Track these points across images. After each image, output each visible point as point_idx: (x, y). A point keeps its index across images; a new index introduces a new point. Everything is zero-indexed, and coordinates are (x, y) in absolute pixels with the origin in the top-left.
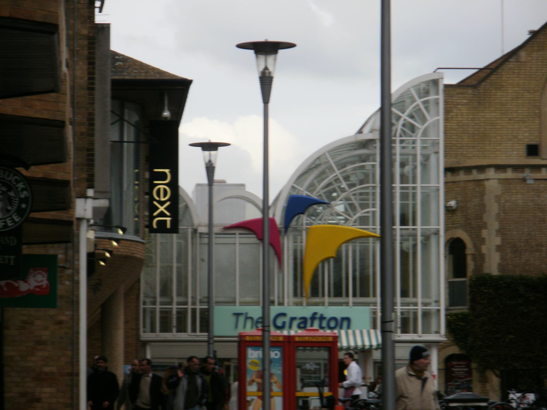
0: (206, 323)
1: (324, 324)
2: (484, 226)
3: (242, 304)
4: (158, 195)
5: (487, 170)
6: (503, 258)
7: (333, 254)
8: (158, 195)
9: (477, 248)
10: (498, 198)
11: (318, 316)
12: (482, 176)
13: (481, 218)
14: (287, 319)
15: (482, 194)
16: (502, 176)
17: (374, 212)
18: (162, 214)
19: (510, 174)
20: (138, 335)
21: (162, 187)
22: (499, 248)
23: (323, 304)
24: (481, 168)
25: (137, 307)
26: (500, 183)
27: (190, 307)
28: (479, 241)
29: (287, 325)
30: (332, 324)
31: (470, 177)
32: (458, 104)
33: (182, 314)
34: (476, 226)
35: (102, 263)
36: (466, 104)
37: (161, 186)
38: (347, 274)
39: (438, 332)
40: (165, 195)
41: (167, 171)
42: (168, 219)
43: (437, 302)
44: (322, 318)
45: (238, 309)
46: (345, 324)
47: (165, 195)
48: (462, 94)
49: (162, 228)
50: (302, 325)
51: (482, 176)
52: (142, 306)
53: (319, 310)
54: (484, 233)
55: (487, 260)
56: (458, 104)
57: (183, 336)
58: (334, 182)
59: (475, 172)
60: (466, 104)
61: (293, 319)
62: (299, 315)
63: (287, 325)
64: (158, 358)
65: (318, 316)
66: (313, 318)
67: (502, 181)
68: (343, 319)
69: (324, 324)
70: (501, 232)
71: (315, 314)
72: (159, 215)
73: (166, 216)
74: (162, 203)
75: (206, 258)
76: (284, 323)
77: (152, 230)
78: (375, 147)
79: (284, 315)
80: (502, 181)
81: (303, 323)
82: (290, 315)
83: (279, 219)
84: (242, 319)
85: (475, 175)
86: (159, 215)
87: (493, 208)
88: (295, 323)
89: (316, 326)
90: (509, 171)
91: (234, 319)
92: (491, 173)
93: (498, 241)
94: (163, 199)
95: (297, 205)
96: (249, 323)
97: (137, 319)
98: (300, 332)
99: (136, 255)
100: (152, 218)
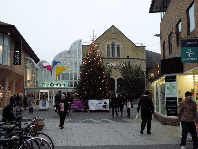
1: (60, 85)
7: (52, 70)
18: (17, 61)
35: (123, 103)
37: (17, 55)
38: (7, 57)
41: (19, 52)
44: (59, 84)
49: (17, 64)
66: (58, 84)
69: (60, 85)
72: (16, 61)
74: (17, 58)
77: (15, 64)
78: (179, 104)
82: (53, 83)
83: (51, 66)
84: (44, 84)
86: (16, 61)
88: (54, 85)
89: (58, 85)
95: (55, 63)
96: (45, 85)
97: (23, 85)
98: (55, 87)
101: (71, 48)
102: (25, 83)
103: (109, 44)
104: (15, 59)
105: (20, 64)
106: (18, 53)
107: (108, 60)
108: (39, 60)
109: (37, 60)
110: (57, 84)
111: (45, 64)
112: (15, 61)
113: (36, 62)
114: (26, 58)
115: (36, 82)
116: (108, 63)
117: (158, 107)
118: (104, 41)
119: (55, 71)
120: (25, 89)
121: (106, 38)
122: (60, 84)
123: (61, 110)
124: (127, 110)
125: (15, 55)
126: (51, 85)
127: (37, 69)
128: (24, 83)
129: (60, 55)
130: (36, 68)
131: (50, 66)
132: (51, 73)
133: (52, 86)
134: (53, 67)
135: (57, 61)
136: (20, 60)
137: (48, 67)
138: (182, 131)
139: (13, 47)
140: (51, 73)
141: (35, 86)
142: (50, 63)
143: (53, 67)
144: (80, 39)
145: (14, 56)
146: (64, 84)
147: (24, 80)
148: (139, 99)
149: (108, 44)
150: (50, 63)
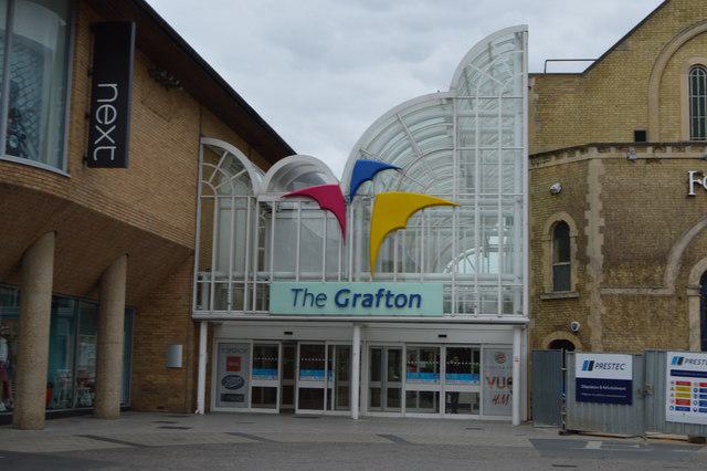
0: (263, 301)
1: (392, 302)
2: (587, 207)
3: (301, 279)
4: (102, 119)
5: (590, 149)
6: (607, 240)
7: (351, 209)
9: (581, 230)
10: (602, 179)
11: (385, 293)
12: (585, 156)
13: (584, 199)
15: (586, 174)
16: (605, 155)
18: (105, 142)
19: (613, 153)
20: (190, 312)
21: (107, 106)
22: (601, 230)
23: (391, 279)
24: (583, 149)
25: (191, 282)
26: (603, 163)
27: (246, 281)
28: (583, 223)
30: (401, 302)
31: (574, 159)
32: (565, 92)
34: (579, 209)
36: (572, 92)
37: (107, 105)
39: (521, 313)
40: (109, 119)
41: (114, 86)
43: (521, 278)
44: (389, 295)
45: (297, 284)
47: (109, 119)
48: (569, 82)
49: (104, 161)
50: (367, 303)
51: (585, 156)
52: (196, 281)
53: (387, 286)
54: (587, 215)
55: (590, 241)
56: (565, 92)
57: (237, 314)
58: (378, 384)
59: (578, 153)
60: (572, 92)
61: (356, 296)
62: (363, 293)
65: (385, 293)
66: (379, 295)
67: (605, 161)
68: (412, 297)
69: (392, 302)
70: (605, 213)
71: (381, 290)
72: (100, 144)
73: (111, 144)
74: (105, 128)
79: (348, 291)
80: (605, 161)
81: (368, 301)
83: (345, 190)
84: (301, 296)
85: (578, 156)
86: (100, 144)
87: (595, 189)
90: (613, 149)
91: (294, 294)
92: (593, 153)
93: (602, 222)
94: (107, 123)
95: (365, 171)
96: (309, 300)
97: (191, 295)
99: (26, 185)
100: (92, 147)
101: (465, 76)
102: (199, 285)
104: (93, 134)
105: (120, 161)
106: (109, 93)
107: (700, 155)
109: (267, 146)
110: (374, 292)
112: (92, 147)
114: (205, 146)
115: (255, 282)
116: (699, 175)
117: (260, 246)
118: (675, 45)
120: (197, 323)
121: (687, 29)
124: (521, 91)
125: (95, 105)
126: (342, 301)
127: (266, 207)
128: (191, 286)
129: (399, 118)
130: (261, 198)
131: (336, 189)
132: (344, 232)
134: (353, 193)
135: (375, 155)
136: (121, 135)
137: (329, 199)
138: (529, 265)
139: (82, 54)
140: (344, 232)
142: (336, 167)
143: (353, 193)
144: (514, 20)
145: (90, 117)
147: (196, 273)
149: (693, 61)
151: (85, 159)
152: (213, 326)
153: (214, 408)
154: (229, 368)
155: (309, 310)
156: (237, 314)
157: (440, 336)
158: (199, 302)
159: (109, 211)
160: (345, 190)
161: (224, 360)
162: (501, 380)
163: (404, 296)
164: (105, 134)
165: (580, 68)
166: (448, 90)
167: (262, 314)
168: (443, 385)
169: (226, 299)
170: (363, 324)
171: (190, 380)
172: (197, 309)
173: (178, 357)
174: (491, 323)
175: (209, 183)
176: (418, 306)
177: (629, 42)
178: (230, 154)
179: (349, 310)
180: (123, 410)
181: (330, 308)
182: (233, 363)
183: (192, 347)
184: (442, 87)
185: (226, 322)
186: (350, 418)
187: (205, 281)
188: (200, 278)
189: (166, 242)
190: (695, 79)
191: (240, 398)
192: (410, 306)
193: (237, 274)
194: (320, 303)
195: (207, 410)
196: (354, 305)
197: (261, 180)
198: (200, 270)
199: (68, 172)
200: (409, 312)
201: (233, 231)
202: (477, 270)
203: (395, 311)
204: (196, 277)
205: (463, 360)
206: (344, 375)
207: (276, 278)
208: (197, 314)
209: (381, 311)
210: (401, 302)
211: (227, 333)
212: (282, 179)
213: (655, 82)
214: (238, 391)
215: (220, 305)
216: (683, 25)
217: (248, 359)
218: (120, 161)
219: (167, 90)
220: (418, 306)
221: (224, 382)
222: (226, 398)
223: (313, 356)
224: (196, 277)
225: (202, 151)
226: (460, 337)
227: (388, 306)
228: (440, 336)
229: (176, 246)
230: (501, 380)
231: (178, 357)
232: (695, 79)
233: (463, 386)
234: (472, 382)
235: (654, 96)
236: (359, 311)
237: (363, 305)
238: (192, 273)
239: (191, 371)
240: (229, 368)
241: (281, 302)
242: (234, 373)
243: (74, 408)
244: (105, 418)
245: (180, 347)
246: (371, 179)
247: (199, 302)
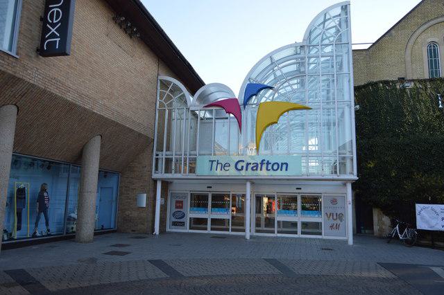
1: (270, 167)
4: (52, 19)
8: (52, 19)
11: (265, 162)
14: (244, 164)
17: (228, 230)
18: (53, 36)
21: (55, 10)
29: (245, 168)
30: (275, 167)
33: (168, 161)
39: (352, 173)
40: (53, 12)
42: (58, 40)
44: (268, 163)
46: (284, 166)
47: (53, 12)
57: (178, 176)
58: (259, 215)
61: (248, 164)
63: (245, 168)
64: (350, 89)
66: (262, 163)
69: (270, 167)
72: (49, 38)
73: (57, 37)
74: (53, 25)
75: (309, 177)
76: (243, 167)
83: (241, 101)
94: (55, 22)
95: (253, 89)
96: (219, 166)
100: (43, 40)
101: (310, 33)
102: (157, 160)
103: (436, 40)
108: (201, 84)
109: (193, 82)
111: (221, 97)
112: (43, 40)
113: (193, 93)
114: (161, 80)
115: (188, 157)
119: (248, 115)
120: (155, 181)
121: (426, 23)
122: (272, 161)
123: (419, 207)
125: (47, 9)
126: (239, 167)
129: (272, 61)
130: (192, 108)
131: (233, 101)
133: (242, 169)
134: (245, 104)
135: (259, 80)
137: (231, 107)
141: (185, 172)
142: (237, 90)
143: (245, 104)
145: (44, 20)
146: (287, 164)
148: (397, 227)
149: (430, 40)
150: (237, 90)
151: (38, 50)
152: (166, 184)
153: (168, 229)
154: (177, 207)
155: (219, 172)
156: (178, 176)
157: (297, 189)
158: (157, 169)
159: (70, 97)
160: (241, 101)
161: (174, 202)
162: (335, 214)
163: (277, 164)
164: (53, 30)
165: (366, 47)
166: (301, 41)
167: (192, 176)
168: (299, 218)
169: (171, 166)
170: (253, 182)
171: (150, 215)
172: (155, 173)
173: (143, 201)
174: (333, 180)
175: (162, 101)
176: (286, 170)
177: (393, 32)
178: (174, 84)
179: (243, 172)
180: (95, 234)
181: (232, 172)
182: (179, 204)
183: (152, 195)
184: (299, 38)
185: (176, 181)
186: (244, 237)
187: (160, 157)
188: (157, 155)
189: (131, 131)
190: (430, 50)
191: (182, 224)
192: (281, 170)
193: (178, 153)
194: (226, 168)
195: (163, 230)
196: (247, 169)
197: (191, 100)
198: (157, 150)
199: (17, 54)
200: (280, 174)
201: (181, 128)
202: (318, 149)
203: (272, 173)
204: (154, 155)
205: (312, 203)
206: (241, 210)
207: (199, 155)
208: (155, 176)
209: (263, 173)
210: (275, 167)
211: (176, 189)
212: (202, 98)
213: (409, 52)
214: (181, 220)
215: (168, 170)
216: (423, 21)
217: (187, 202)
218: (63, 52)
219: (131, 37)
220: (286, 170)
221: (174, 215)
222: (175, 224)
223: (219, 201)
224: (154, 155)
225: (159, 84)
226: (309, 190)
227: (267, 169)
228: (297, 189)
229: (140, 135)
230: (335, 214)
231: (143, 201)
232: (430, 50)
233: (312, 218)
234: (317, 216)
235: (408, 59)
236: (249, 174)
237: (252, 169)
238: (153, 152)
239: (151, 210)
240: (177, 207)
241: (203, 169)
242: (179, 210)
243: (65, 234)
244: (82, 242)
245: (145, 196)
246: (256, 95)
247: (157, 169)
